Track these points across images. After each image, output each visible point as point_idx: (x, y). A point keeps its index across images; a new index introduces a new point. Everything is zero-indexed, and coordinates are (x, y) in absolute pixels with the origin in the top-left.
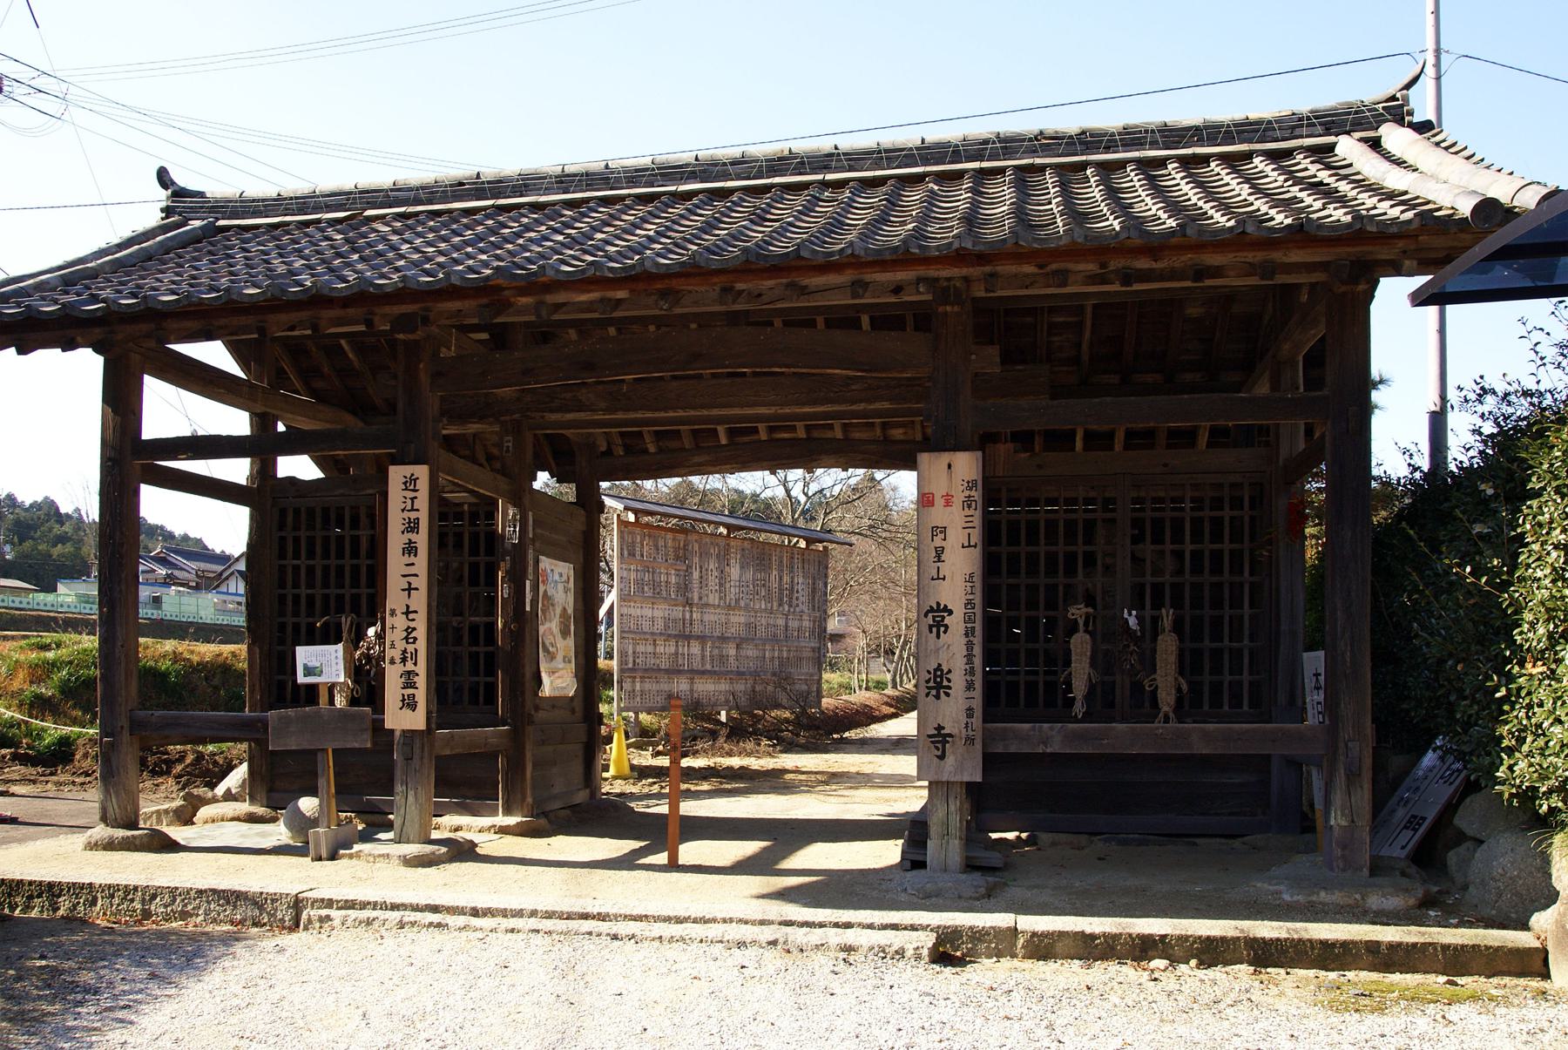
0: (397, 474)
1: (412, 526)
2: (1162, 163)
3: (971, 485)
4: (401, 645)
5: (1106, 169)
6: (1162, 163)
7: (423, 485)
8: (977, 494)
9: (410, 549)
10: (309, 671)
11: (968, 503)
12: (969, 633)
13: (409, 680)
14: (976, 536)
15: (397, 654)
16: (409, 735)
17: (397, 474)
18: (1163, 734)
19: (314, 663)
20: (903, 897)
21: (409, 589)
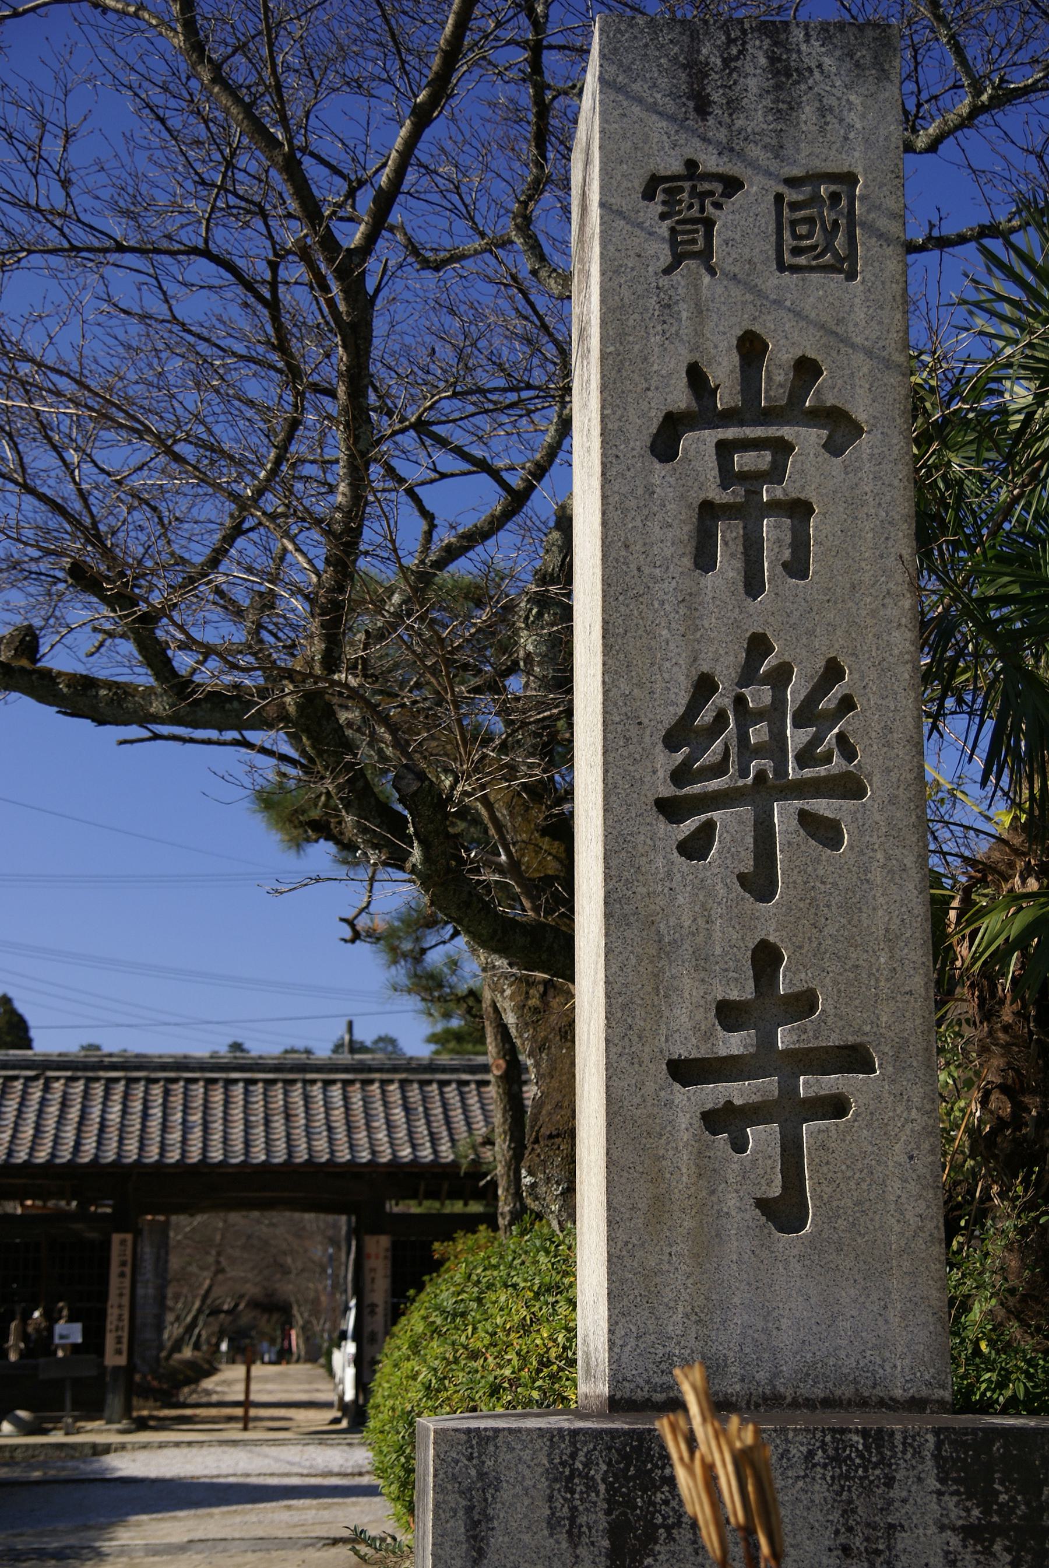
0: (116, 1238)
1: (123, 1264)
2: (467, 1083)
3: (387, 1250)
4: (115, 1323)
5: (443, 1084)
6: (467, 1083)
7: (130, 1243)
8: (389, 1254)
9: (122, 1275)
10: (62, 1337)
11: (386, 1258)
12: (386, 1315)
13: (119, 1340)
14: (389, 1273)
15: (113, 1327)
16: (117, 1369)
17: (116, 1238)
18: (857, 1421)
19: (64, 1332)
20: (620, 1332)
21: (121, 1295)
